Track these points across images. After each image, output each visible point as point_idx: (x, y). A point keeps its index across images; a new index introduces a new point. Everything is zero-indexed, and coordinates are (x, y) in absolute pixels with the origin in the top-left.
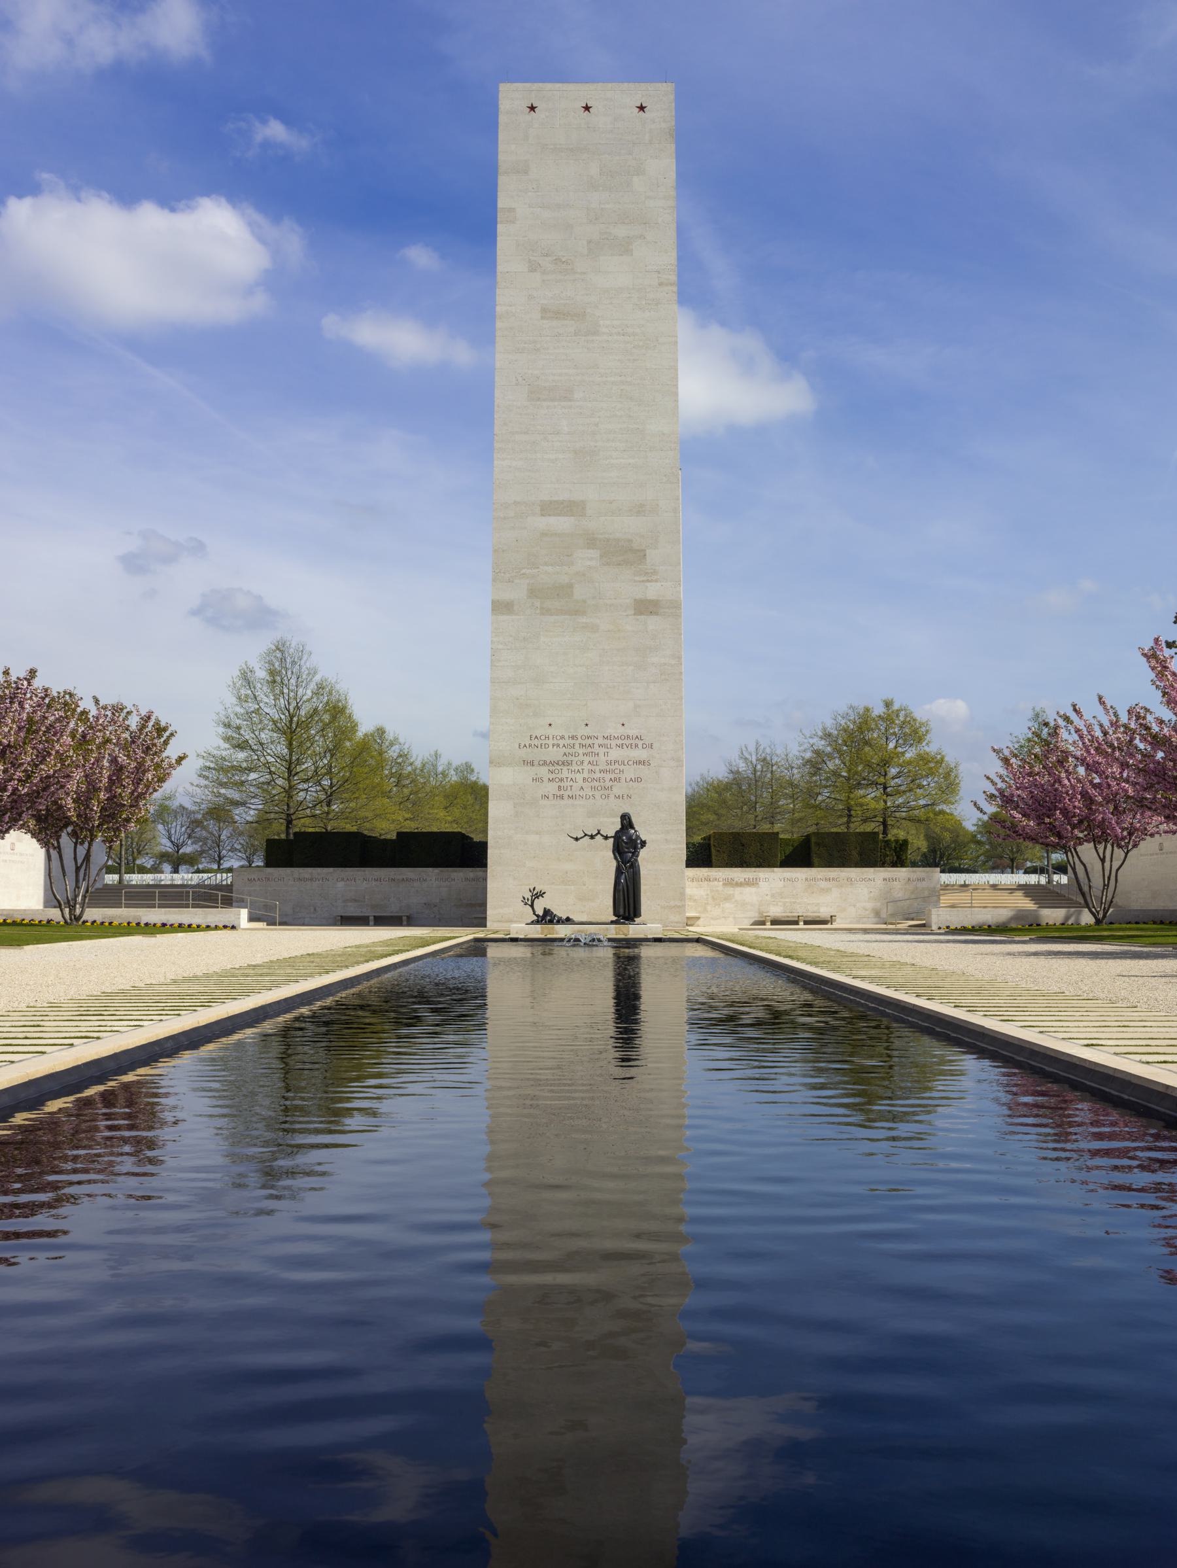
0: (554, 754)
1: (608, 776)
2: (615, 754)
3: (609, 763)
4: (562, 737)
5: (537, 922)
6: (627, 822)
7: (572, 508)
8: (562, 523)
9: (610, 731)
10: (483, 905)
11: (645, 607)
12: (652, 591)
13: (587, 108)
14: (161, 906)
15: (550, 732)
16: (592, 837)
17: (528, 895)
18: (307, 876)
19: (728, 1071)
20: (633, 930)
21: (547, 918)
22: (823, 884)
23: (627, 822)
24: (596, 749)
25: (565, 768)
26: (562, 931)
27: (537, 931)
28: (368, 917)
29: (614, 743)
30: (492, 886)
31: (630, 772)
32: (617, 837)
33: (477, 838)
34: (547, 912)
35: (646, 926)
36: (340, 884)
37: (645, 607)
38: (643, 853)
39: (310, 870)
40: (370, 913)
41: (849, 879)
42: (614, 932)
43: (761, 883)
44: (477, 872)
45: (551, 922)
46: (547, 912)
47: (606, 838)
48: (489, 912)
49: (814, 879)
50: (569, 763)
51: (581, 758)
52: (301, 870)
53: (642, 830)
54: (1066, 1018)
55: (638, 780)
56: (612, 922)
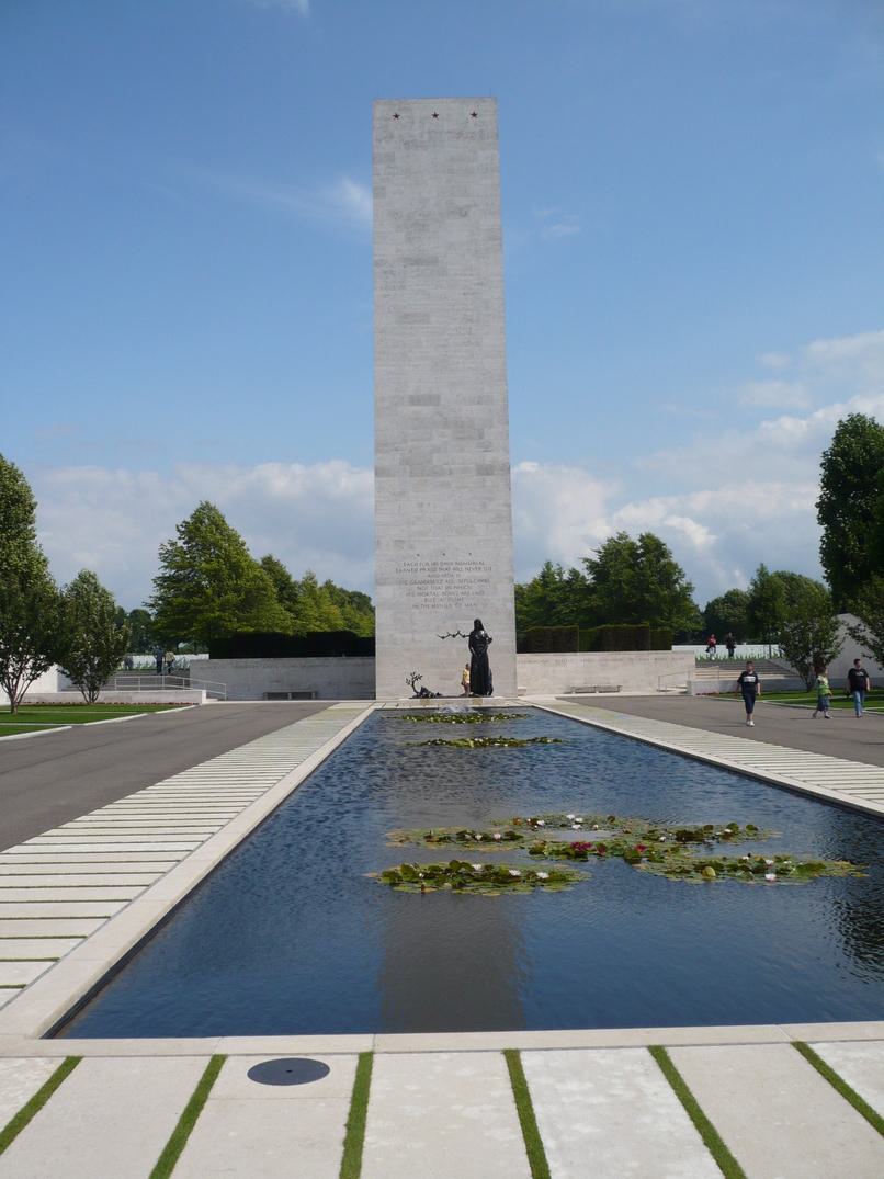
0: (422, 576)
1: (460, 591)
2: (465, 575)
3: (460, 582)
4: (427, 564)
5: (417, 697)
6: (478, 625)
7: (432, 400)
8: (426, 411)
9: (460, 559)
10: (373, 686)
11: (485, 471)
12: (489, 458)
13: (435, 116)
14: (167, 688)
15: (419, 560)
16: (454, 636)
17: (410, 678)
18: (243, 664)
19: (613, 1045)
20: (485, 702)
21: (424, 694)
22: (612, 663)
23: (478, 625)
24: (451, 572)
25: (429, 586)
26: (433, 704)
27: (418, 704)
28: (310, 693)
29: (463, 567)
30: (379, 669)
31: (476, 587)
32: (472, 636)
33: (365, 634)
34: (424, 690)
35: (496, 699)
36: (267, 670)
37: (485, 471)
38: (490, 646)
39: (244, 660)
40: (286, 689)
41: (631, 660)
42: (472, 703)
43: (568, 664)
44: (367, 660)
45: (427, 696)
46: (424, 690)
47: (464, 637)
48: (377, 689)
49: (606, 660)
50: (433, 582)
51: (441, 578)
52: (238, 660)
53: (488, 630)
54: (194, 823)
55: (482, 593)
56: (462, 696)
